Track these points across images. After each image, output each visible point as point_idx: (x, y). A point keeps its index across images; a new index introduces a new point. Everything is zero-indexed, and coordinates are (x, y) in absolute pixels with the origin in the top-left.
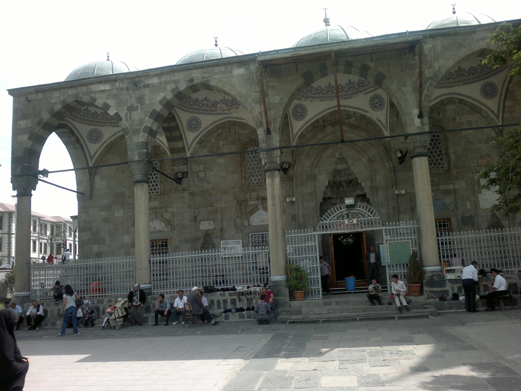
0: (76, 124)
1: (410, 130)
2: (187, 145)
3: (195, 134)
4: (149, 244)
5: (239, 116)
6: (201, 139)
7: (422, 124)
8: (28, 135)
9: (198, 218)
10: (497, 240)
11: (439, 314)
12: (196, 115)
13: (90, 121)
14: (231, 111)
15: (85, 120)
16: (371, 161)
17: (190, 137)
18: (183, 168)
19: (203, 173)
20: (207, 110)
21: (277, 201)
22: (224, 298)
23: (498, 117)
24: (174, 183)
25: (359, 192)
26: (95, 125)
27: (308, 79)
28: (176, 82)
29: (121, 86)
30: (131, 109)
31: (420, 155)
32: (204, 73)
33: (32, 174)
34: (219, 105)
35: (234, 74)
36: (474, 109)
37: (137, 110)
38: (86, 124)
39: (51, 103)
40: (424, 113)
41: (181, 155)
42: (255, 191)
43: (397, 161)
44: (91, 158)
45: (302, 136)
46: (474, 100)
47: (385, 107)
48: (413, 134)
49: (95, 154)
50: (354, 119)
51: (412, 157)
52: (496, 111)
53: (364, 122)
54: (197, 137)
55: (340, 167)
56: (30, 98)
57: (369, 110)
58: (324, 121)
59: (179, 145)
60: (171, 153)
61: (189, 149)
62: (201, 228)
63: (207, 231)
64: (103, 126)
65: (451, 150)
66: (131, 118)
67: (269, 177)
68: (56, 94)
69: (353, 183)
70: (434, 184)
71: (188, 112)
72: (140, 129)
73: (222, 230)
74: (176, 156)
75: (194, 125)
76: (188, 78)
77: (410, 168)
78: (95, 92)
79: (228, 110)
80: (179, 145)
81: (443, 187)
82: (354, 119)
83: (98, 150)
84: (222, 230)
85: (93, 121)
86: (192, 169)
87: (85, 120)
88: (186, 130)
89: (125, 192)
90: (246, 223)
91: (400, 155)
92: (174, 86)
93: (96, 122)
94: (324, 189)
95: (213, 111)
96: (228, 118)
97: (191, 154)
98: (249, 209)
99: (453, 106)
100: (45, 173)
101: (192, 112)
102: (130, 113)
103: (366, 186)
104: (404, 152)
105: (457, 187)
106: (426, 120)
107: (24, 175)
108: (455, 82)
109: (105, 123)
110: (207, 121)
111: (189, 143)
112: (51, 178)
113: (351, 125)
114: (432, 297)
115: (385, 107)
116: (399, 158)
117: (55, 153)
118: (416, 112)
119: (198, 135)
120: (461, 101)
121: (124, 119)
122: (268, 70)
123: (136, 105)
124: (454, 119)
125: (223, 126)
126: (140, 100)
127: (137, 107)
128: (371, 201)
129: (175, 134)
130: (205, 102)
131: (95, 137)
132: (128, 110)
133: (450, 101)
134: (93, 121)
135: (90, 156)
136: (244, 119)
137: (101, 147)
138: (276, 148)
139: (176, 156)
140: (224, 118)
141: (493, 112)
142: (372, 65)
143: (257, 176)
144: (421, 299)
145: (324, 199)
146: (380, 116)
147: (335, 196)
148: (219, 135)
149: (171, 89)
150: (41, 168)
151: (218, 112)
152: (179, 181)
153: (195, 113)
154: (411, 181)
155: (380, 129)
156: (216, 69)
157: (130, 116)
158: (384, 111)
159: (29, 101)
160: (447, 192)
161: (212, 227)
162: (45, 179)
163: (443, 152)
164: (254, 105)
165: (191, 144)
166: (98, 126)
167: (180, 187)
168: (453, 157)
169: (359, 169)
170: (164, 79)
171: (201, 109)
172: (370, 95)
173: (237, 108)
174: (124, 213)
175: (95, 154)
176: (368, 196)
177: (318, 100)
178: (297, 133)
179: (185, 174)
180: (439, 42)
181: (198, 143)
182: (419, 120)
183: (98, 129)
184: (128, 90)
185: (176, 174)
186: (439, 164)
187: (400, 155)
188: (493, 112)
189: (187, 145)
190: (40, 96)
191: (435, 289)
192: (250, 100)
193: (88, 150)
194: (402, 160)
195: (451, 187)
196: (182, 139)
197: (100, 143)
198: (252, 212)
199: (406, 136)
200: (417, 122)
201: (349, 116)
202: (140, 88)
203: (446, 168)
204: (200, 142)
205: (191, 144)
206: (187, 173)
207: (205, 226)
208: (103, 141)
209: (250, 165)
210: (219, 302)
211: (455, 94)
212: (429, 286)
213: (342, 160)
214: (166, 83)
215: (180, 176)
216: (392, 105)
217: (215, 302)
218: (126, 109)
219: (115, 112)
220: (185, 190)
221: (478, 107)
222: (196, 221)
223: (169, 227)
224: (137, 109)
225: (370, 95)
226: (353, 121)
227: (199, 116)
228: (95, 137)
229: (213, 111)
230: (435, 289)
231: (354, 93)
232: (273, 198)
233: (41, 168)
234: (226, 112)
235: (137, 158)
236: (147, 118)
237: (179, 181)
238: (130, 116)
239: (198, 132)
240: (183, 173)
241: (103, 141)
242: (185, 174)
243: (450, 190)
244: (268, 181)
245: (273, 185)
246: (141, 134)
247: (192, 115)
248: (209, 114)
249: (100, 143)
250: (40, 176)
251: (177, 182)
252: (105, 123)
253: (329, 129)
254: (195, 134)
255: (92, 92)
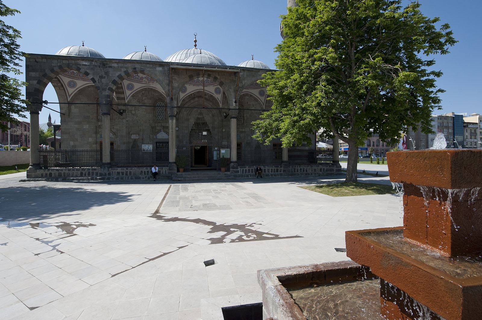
0: (62, 77)
1: (231, 107)
2: (126, 96)
3: (131, 92)
4: (110, 144)
5: (154, 86)
6: (133, 94)
7: (236, 105)
8: (37, 81)
9: (131, 133)
10: (244, 172)
11: (235, 179)
12: (132, 82)
13: (70, 76)
14: (150, 83)
15: (67, 75)
16: (213, 116)
17: (128, 93)
18: (123, 108)
19: (134, 111)
20: (138, 81)
21: (174, 131)
22: (148, 170)
23: (264, 104)
24: (119, 115)
25: (207, 128)
26: (72, 78)
27: (191, 77)
28: (126, 68)
29: (96, 64)
30: (101, 77)
31: (234, 118)
32: (141, 66)
33: (39, 102)
34: (144, 79)
35: (157, 69)
36: (256, 100)
37: (105, 78)
38: (67, 77)
39: (52, 66)
40: (237, 101)
41: (123, 102)
42: (160, 123)
43: (224, 117)
44: (69, 96)
45: (183, 100)
46: (256, 96)
47: (221, 94)
48: (232, 109)
49: (72, 94)
50: (207, 96)
51: (231, 118)
52: (263, 102)
53: (211, 98)
54: (131, 93)
55: (200, 116)
56: (37, 60)
57: (214, 93)
58: (194, 95)
59: (122, 96)
60: (117, 99)
61: (127, 99)
62: (132, 138)
63: (135, 139)
64: (78, 80)
65: (245, 115)
66: (101, 82)
67: (171, 119)
68: (56, 61)
69: (205, 124)
70: (238, 128)
71: (128, 80)
72: (106, 88)
73: (142, 139)
74: (120, 101)
75: (130, 87)
76: (133, 67)
77: (230, 121)
78: (80, 65)
79: (148, 82)
80: (122, 96)
81: (241, 130)
82: (207, 96)
83: (74, 92)
84: (142, 139)
85: (71, 76)
86: (128, 109)
87: (67, 75)
88: (126, 89)
89: (90, 116)
90: (155, 137)
91: (225, 115)
92: (125, 70)
93: (73, 77)
94: (192, 125)
95: (141, 81)
96: (148, 86)
97: (128, 101)
98: (157, 131)
99: (248, 97)
100: (46, 102)
101: (130, 81)
102: (101, 79)
103: (210, 126)
104: (227, 114)
105: (246, 130)
106: (237, 104)
107: (35, 103)
108: (250, 87)
109: (78, 78)
110: (137, 86)
111: (127, 96)
112: (49, 105)
113: (206, 99)
114: (233, 173)
115: (221, 94)
116: (225, 116)
117: (50, 93)
118: (234, 100)
119: (132, 92)
120: (251, 96)
121: (97, 82)
122: (173, 71)
123: (104, 76)
124: (248, 102)
125: (145, 90)
126: (107, 73)
127: (105, 77)
128: (212, 133)
129: (121, 90)
130: (137, 77)
131: (72, 85)
132: (99, 77)
133: (247, 95)
134: (71, 76)
135: (69, 95)
136: (156, 88)
137: (75, 91)
138: (175, 107)
139: (120, 101)
140: (146, 86)
141: (262, 102)
142: (219, 77)
143: (161, 116)
144: (228, 173)
145: (192, 129)
146: (219, 97)
147: (196, 129)
148: (143, 94)
149: (124, 71)
150: (44, 100)
151: (143, 82)
152: (121, 114)
153: (131, 81)
154: (229, 127)
155: (218, 102)
156: (148, 65)
157: (101, 81)
158: (221, 95)
159: (37, 62)
160: (242, 132)
161: (137, 138)
162: (45, 105)
163: (242, 116)
164: (165, 86)
165: (129, 96)
166: (74, 79)
167: (121, 117)
168: (245, 118)
169: (208, 118)
170: (120, 65)
171: (135, 80)
172: (215, 87)
173: (153, 82)
174: (89, 127)
175: (72, 94)
176: (211, 130)
177: (192, 85)
178: (181, 99)
179: (124, 111)
180: (246, 73)
181: (132, 96)
182: (235, 104)
183: (74, 81)
184: (100, 67)
185: (120, 110)
186: (240, 120)
187: (225, 115)
188: (262, 102)
189: (126, 96)
190: (44, 60)
191: (234, 170)
192: (164, 83)
193: (68, 91)
194: (226, 117)
195: (244, 130)
196: (124, 94)
197: (75, 89)
198: (158, 133)
199: (230, 109)
200: (234, 104)
201: (205, 94)
202: (106, 67)
203: (242, 122)
204: (133, 96)
205: (129, 96)
206: (126, 110)
207: (134, 137)
208: (77, 87)
209: (158, 110)
210: (145, 172)
211: (249, 92)
212: (232, 169)
213: (201, 114)
214: (121, 67)
215: (122, 111)
216: (224, 93)
217: (143, 172)
218: (98, 77)
219: (92, 77)
220: (124, 118)
221: (257, 99)
222: (129, 134)
223: (115, 136)
224: (105, 77)
225: (215, 87)
226: (207, 97)
227: (133, 83)
228: (72, 85)
229: (141, 81)
230: (234, 170)
231: (209, 85)
232: (172, 128)
233: (44, 100)
234: (147, 83)
235: (104, 102)
236: (111, 83)
237: (121, 114)
238: (101, 81)
239: (132, 91)
240: (123, 110)
241: (77, 87)
242: (124, 111)
243: (243, 131)
244: (170, 121)
245: (172, 123)
246: (107, 91)
247: (130, 82)
248: (138, 83)
249: (75, 89)
250: (44, 104)
251: (120, 115)
252: (78, 78)
253: (196, 99)
254: (131, 92)
255: (78, 64)
